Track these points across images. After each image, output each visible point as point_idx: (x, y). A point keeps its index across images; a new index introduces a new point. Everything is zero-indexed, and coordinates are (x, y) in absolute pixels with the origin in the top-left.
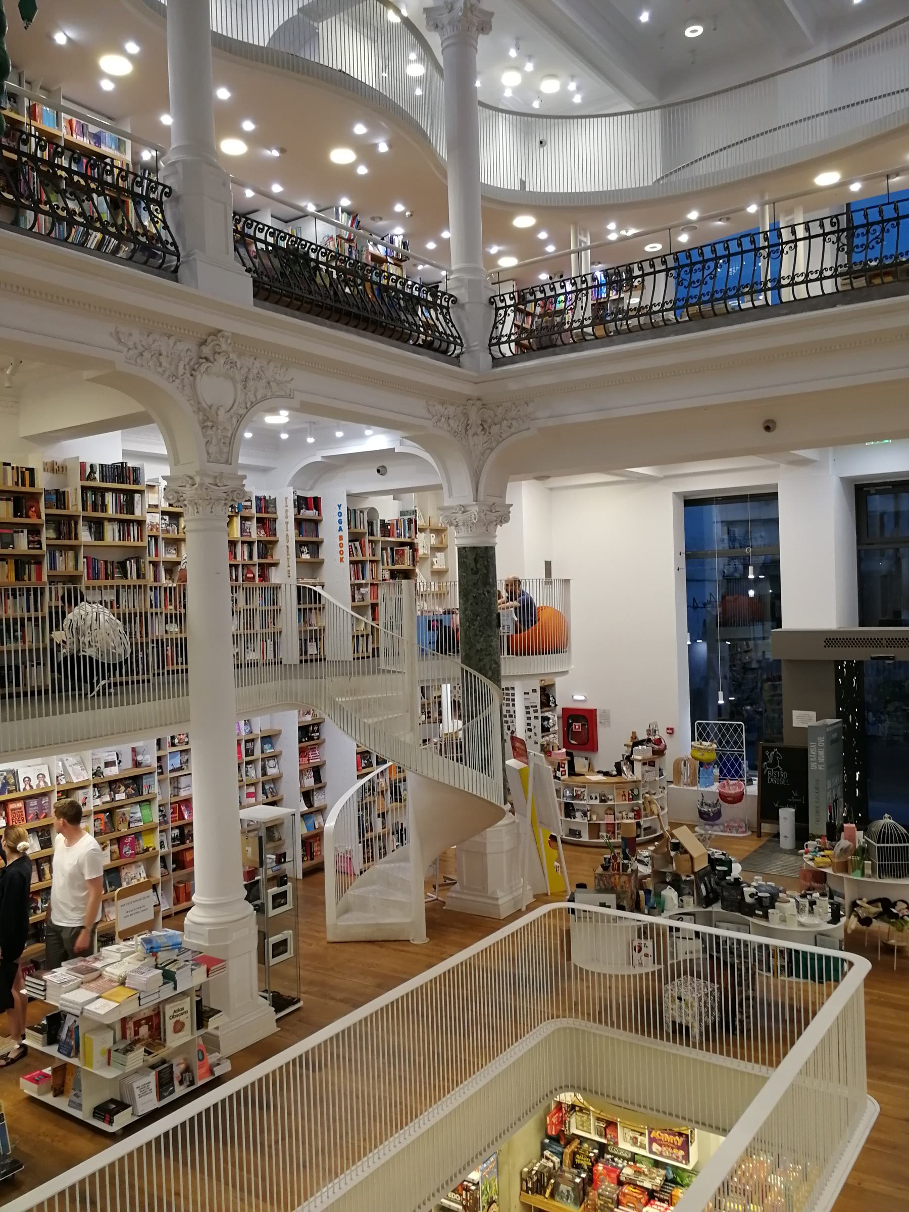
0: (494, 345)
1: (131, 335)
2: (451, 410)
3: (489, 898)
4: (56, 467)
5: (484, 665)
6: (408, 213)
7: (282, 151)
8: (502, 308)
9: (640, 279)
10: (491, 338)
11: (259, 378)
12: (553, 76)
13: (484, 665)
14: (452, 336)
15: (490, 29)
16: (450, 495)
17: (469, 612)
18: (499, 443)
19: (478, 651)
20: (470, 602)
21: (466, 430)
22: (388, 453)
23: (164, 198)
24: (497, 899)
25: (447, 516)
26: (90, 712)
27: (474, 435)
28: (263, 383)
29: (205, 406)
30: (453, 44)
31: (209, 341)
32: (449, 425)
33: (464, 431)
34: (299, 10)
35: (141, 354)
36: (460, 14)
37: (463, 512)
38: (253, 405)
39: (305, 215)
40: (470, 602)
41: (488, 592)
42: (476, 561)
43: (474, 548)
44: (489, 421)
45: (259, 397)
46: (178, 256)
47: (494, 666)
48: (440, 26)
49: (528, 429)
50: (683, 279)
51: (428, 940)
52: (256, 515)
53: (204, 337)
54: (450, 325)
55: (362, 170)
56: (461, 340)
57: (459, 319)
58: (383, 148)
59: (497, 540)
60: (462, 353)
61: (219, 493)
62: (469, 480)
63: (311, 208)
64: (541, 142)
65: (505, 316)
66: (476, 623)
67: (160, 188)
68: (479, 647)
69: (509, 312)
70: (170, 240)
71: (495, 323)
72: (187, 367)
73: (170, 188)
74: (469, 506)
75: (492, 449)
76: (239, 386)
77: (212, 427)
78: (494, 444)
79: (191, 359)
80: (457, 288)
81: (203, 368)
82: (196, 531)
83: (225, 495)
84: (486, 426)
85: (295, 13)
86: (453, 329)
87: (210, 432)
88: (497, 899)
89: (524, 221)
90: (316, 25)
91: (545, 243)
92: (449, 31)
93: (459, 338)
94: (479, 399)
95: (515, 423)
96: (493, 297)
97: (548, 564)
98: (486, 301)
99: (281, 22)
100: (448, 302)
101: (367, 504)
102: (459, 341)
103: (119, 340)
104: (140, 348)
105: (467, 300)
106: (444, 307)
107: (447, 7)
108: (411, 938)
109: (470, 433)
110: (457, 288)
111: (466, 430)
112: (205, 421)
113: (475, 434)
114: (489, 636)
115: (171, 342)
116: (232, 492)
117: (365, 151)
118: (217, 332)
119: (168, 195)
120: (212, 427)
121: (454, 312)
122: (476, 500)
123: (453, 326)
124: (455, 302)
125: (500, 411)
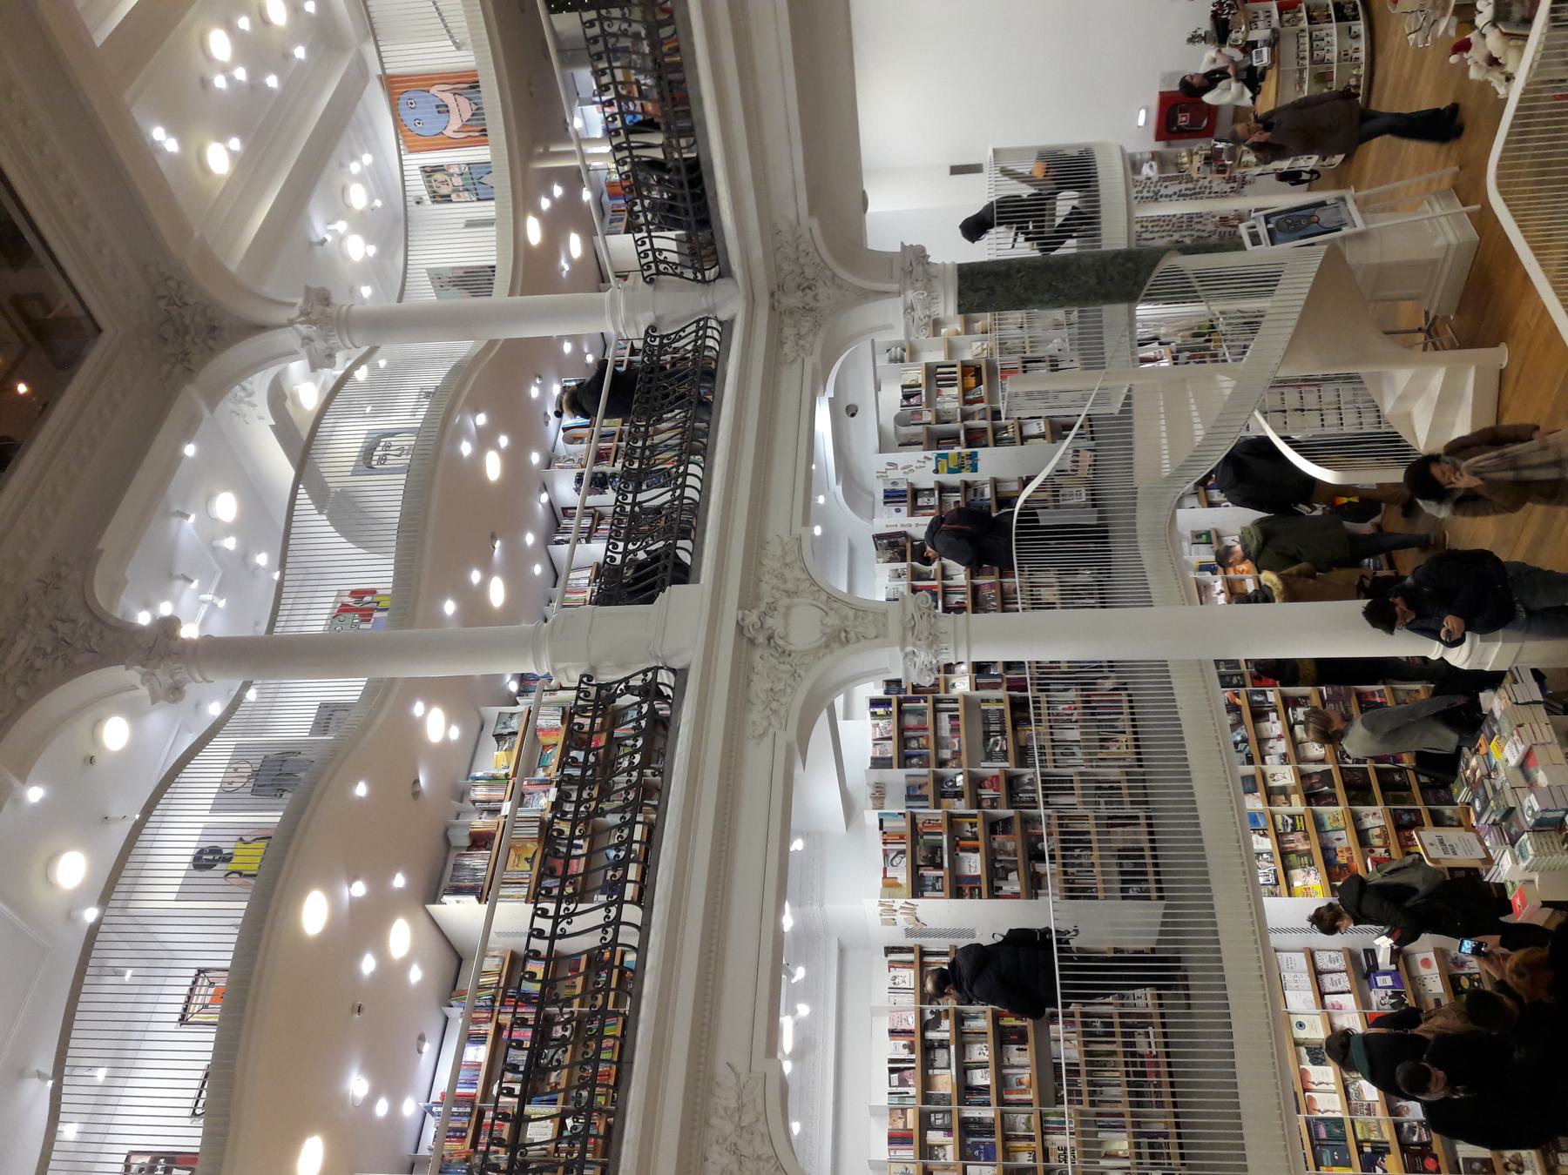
0: (704, 276)
1: (754, 723)
2: (788, 332)
3: (1447, 254)
4: (877, 795)
5: (1119, 273)
6: (538, 381)
7: (493, 537)
8: (657, 267)
9: (619, 87)
10: (695, 279)
11: (782, 577)
12: (344, 190)
13: (1119, 273)
14: (697, 332)
15: (324, 289)
16: (889, 327)
17: (1046, 298)
18: (826, 267)
19: (1098, 283)
20: (1032, 296)
21: (811, 310)
22: (833, 403)
23: (593, 682)
24: (1449, 245)
25: (917, 331)
26: (1193, 776)
27: (817, 300)
28: (787, 572)
29: (824, 639)
30: (349, 335)
31: (749, 635)
32: (807, 334)
33: (812, 313)
34: (320, 513)
35: (774, 712)
36: (315, 328)
37: (913, 309)
38: (814, 584)
39: (551, 504)
40: (1032, 296)
41: (1018, 272)
42: (976, 290)
43: (961, 294)
44: (799, 280)
45: (804, 576)
46: (658, 668)
47: (1120, 260)
48: (328, 352)
49: (810, 230)
50: (620, 29)
51: (1503, 345)
52: (909, 562)
53: (745, 640)
54: (682, 334)
55: (504, 441)
56: (700, 320)
57: (676, 322)
58: (481, 419)
59: (948, 262)
60: (716, 319)
61: (922, 625)
62: (879, 302)
63: (544, 498)
64: (418, 203)
65: (668, 263)
66: (1061, 286)
67: (583, 686)
68: (1093, 281)
69: (662, 258)
70: (641, 676)
71: (675, 275)
72: (782, 660)
73: (582, 676)
74: (905, 304)
75: (834, 275)
76: (796, 600)
77: (845, 631)
78: (828, 273)
79: (772, 655)
80: (636, 327)
81: (781, 642)
82: (969, 652)
83: (925, 617)
84: (806, 285)
85: (324, 517)
86: (688, 330)
87: (852, 635)
88: (1449, 245)
89: (534, 232)
90: (332, 495)
91: (550, 195)
92: (335, 340)
93: (698, 322)
94: (772, 294)
95: (802, 247)
96: (644, 279)
97: (956, 170)
98: (650, 288)
99: (332, 529)
100: (655, 337)
101: (890, 425)
102: (702, 323)
103: (762, 736)
104: (768, 712)
105: (652, 313)
106: (661, 342)
107: (308, 344)
108: (1499, 368)
109: (813, 304)
110: (636, 327)
111: (811, 310)
112: (840, 641)
113: (815, 298)
114: (1080, 267)
115: (755, 678)
116: (920, 609)
117: (485, 440)
118: (740, 628)
119: (590, 678)
120: (845, 631)
121: (666, 329)
122: (899, 294)
123: (683, 330)
124: (653, 328)
125: (787, 267)
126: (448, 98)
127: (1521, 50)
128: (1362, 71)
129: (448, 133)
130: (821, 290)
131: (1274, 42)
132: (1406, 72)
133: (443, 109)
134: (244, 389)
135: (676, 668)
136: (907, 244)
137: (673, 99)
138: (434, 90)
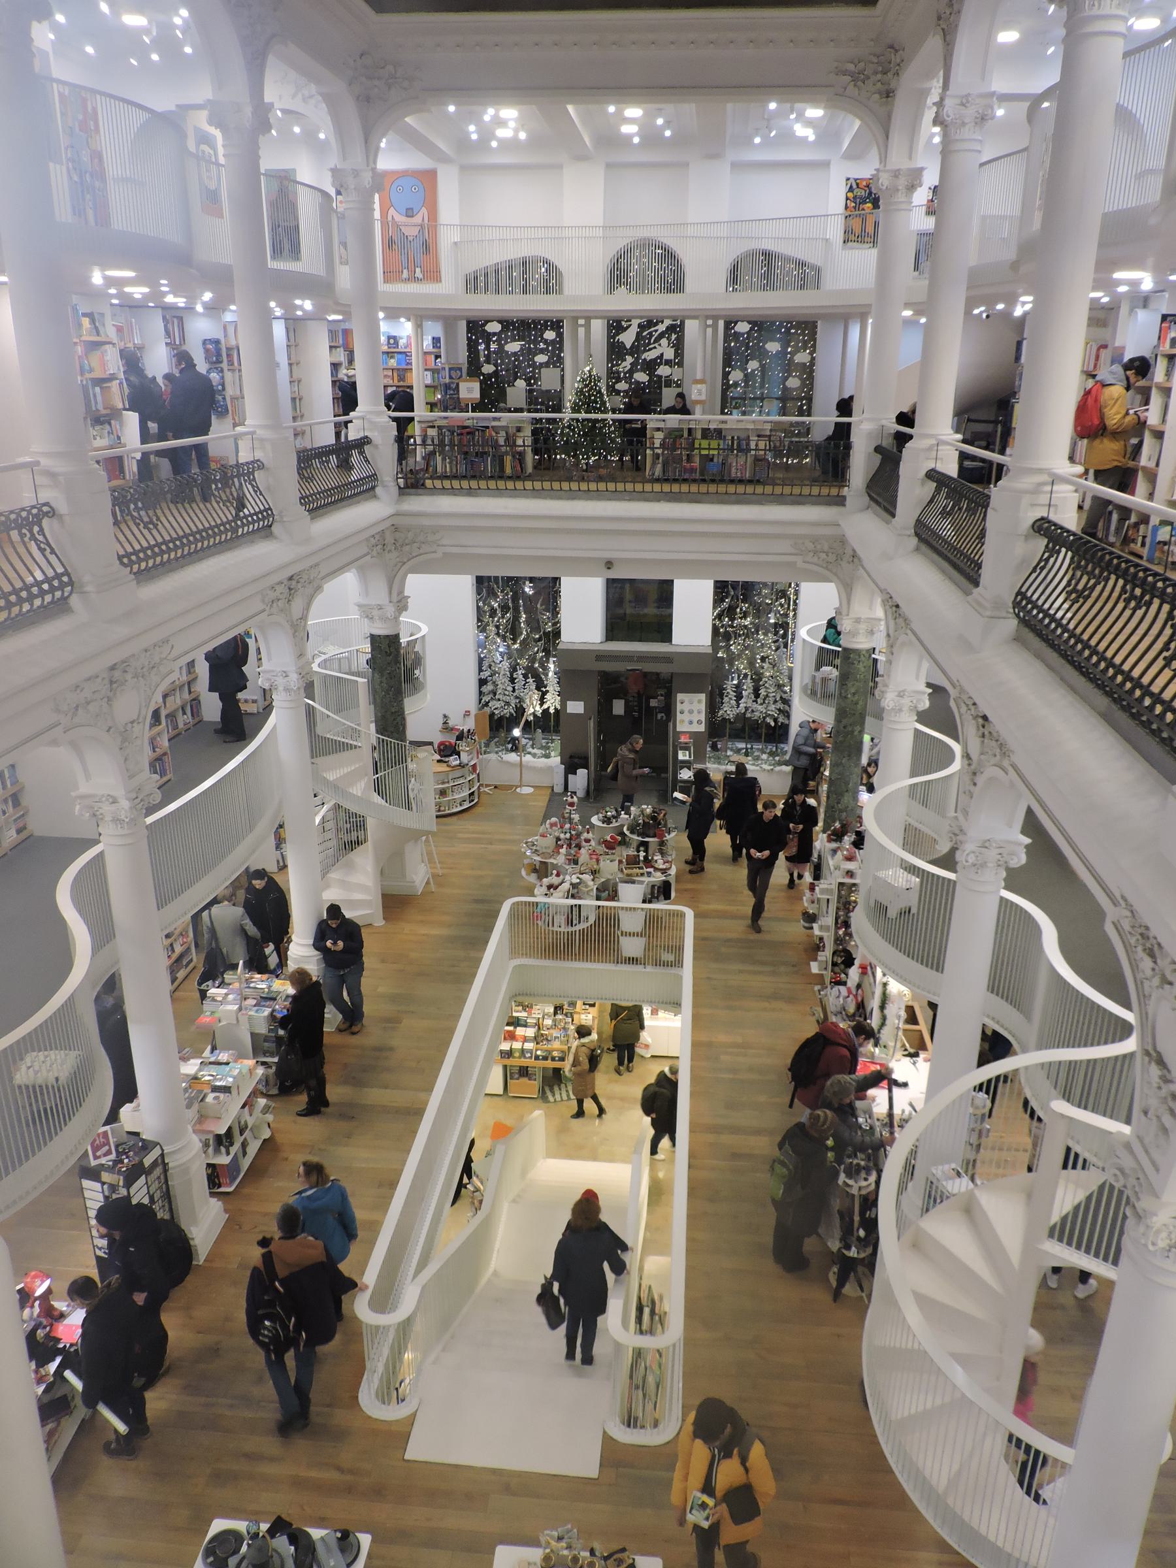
51: (384, 922)
95: (423, 546)
113: (390, 551)
126: (417, 219)
127: (563, 897)
128: (447, 812)
129: (392, 211)
130: (395, 554)
131: (462, 766)
132: (460, 835)
133: (410, 213)
134: (311, 97)
135: (272, 528)
136: (409, 600)
137: (462, 434)
138: (424, 210)
